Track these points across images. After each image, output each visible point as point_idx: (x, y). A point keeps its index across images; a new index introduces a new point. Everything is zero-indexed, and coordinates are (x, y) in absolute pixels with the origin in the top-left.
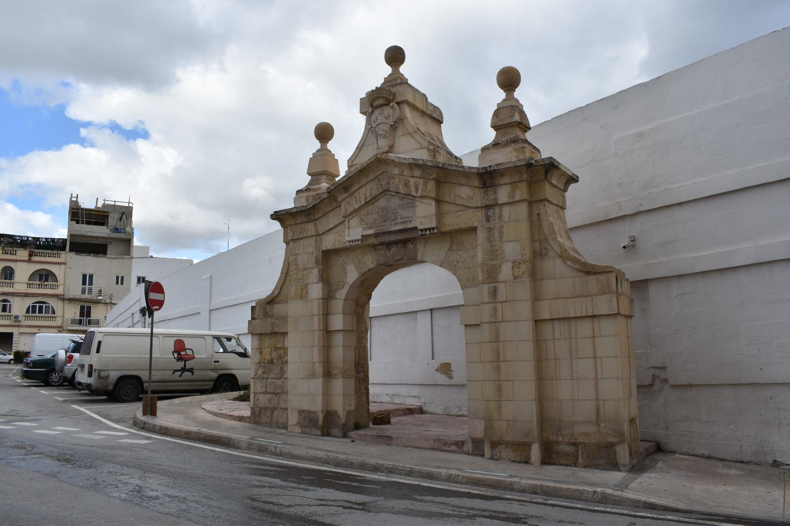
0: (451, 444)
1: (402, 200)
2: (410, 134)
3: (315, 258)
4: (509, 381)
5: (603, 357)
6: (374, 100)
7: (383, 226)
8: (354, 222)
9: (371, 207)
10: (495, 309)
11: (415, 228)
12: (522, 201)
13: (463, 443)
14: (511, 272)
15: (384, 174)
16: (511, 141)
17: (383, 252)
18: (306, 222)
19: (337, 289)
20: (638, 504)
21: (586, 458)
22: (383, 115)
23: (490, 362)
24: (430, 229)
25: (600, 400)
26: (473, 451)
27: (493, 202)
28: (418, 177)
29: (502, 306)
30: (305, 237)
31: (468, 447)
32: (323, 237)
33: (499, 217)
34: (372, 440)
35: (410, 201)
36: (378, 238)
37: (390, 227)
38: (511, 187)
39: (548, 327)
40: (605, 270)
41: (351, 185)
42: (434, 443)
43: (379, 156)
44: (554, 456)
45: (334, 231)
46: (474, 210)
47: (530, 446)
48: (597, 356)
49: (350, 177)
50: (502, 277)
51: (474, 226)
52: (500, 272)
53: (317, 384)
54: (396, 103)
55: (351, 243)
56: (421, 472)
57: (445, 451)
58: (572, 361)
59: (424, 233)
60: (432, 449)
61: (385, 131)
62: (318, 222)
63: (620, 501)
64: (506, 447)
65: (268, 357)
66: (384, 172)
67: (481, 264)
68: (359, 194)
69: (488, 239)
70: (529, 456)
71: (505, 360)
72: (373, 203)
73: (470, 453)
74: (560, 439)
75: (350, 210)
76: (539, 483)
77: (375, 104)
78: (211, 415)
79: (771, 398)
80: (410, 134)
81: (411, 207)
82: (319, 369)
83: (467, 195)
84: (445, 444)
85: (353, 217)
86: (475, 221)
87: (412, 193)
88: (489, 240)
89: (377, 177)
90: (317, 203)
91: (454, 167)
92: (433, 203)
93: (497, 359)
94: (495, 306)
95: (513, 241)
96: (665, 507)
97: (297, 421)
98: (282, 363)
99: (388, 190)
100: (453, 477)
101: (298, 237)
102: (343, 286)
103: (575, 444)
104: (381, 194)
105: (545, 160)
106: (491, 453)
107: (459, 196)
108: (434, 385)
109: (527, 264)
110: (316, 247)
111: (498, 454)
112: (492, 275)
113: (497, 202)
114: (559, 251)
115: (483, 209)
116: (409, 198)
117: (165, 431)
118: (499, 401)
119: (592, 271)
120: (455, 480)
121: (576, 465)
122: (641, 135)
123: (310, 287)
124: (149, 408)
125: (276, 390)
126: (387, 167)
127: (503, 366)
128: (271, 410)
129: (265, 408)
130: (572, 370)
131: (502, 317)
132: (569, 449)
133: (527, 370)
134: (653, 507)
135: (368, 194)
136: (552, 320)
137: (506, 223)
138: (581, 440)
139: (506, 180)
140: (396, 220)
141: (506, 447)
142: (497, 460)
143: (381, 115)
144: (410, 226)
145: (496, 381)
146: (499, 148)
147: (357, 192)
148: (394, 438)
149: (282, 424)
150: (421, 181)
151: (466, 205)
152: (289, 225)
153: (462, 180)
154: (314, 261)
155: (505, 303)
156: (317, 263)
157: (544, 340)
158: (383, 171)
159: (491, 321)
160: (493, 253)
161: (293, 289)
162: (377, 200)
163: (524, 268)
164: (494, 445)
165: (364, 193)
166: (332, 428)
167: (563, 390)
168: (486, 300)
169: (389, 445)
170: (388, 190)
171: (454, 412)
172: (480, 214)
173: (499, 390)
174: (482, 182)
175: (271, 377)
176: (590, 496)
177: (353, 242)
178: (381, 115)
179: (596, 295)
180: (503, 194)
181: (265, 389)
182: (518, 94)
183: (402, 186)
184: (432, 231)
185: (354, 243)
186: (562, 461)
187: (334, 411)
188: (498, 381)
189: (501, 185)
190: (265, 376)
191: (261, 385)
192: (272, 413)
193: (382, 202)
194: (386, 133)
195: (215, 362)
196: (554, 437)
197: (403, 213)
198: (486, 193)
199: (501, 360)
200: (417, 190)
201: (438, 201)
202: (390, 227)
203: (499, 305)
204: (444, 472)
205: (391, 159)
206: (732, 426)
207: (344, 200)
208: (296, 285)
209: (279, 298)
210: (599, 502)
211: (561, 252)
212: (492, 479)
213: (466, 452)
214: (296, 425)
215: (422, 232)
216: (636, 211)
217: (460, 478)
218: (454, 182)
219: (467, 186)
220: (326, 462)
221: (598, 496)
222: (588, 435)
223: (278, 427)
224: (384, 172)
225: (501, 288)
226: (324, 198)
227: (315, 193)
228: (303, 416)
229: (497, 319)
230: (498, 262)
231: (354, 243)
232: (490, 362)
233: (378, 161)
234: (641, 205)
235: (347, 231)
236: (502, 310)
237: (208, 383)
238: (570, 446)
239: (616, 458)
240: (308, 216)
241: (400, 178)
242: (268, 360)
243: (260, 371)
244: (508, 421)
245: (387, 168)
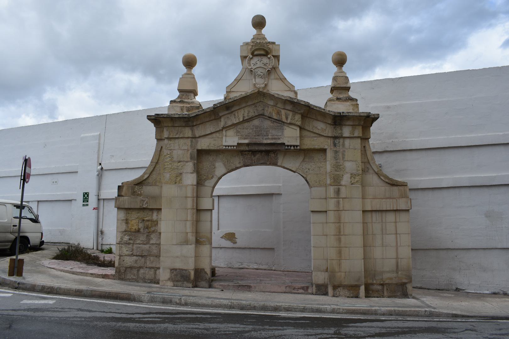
0: (298, 288)
1: (273, 123)
2: (281, 79)
3: (191, 154)
4: (347, 247)
6: (256, 50)
7: (256, 139)
8: (231, 132)
9: (246, 125)
10: (338, 202)
11: (284, 144)
12: (358, 137)
14: (349, 180)
19: (205, 180)
21: (390, 292)
22: (262, 62)
23: (334, 235)
24: (294, 146)
25: (399, 258)
26: (316, 292)
27: (339, 135)
29: (343, 201)
30: (181, 138)
32: (199, 139)
33: (342, 145)
38: (352, 128)
41: (232, 106)
43: (260, 90)
44: (371, 292)
45: (210, 136)
47: (359, 287)
49: (235, 100)
50: (343, 183)
51: (325, 148)
52: (343, 179)
53: (190, 249)
54: (272, 55)
55: (227, 147)
56: (312, 308)
57: (294, 293)
59: (289, 148)
62: (195, 128)
67: (330, 173)
69: (335, 157)
70: (358, 293)
72: (248, 122)
74: (375, 282)
75: (230, 123)
77: (256, 53)
78: (71, 274)
79: (456, 256)
80: (281, 79)
81: (280, 129)
83: (321, 128)
84: (294, 289)
85: (230, 129)
86: (325, 145)
88: (336, 158)
93: (339, 234)
94: (338, 200)
96: (463, 315)
99: (263, 115)
100: (336, 310)
101: (174, 137)
104: (256, 116)
106: (333, 293)
107: (316, 127)
108: (219, 247)
109: (360, 176)
110: (191, 146)
111: (338, 293)
112: (337, 181)
113: (342, 136)
118: (340, 260)
119: (396, 184)
120: (337, 312)
121: (383, 297)
122: (388, 107)
124: (16, 270)
125: (143, 253)
127: (343, 238)
129: (131, 268)
130: (383, 241)
131: (343, 207)
133: (358, 241)
134: (457, 316)
135: (246, 115)
136: (372, 211)
138: (387, 282)
142: (337, 297)
148: (253, 287)
149: (149, 279)
150: (291, 114)
157: (366, 223)
159: (335, 209)
160: (338, 167)
161: (167, 176)
164: (335, 287)
166: (199, 282)
167: (377, 253)
168: (332, 196)
169: (249, 291)
173: (340, 253)
174: (333, 121)
176: (423, 313)
180: (346, 131)
184: (296, 148)
185: (230, 148)
186: (375, 295)
188: (340, 247)
189: (345, 125)
190: (131, 242)
192: (138, 271)
193: (256, 122)
194: (263, 75)
195: (14, 226)
196: (371, 281)
197: (274, 132)
200: (287, 118)
203: (341, 200)
204: (328, 307)
208: (170, 173)
209: (147, 181)
214: (167, 280)
215: (288, 147)
217: (341, 310)
218: (313, 118)
223: (145, 282)
225: (343, 189)
227: (189, 106)
228: (175, 273)
231: (230, 148)
232: (334, 235)
235: (224, 138)
236: (343, 203)
237: (7, 244)
239: (407, 291)
242: (136, 229)
243: (126, 238)
245: (263, 99)
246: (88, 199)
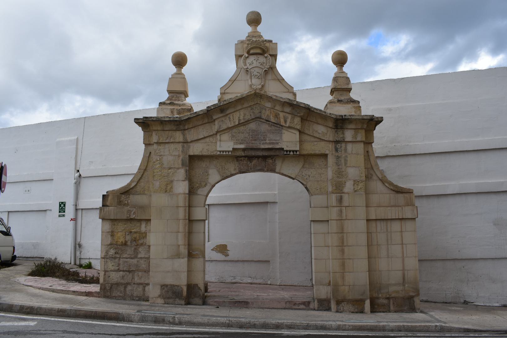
3: (182, 160)
5: (408, 244)
7: (252, 143)
8: (226, 137)
9: (242, 128)
12: (361, 141)
13: (309, 303)
14: (352, 188)
15: (258, 105)
17: (245, 162)
18: (175, 130)
19: (198, 188)
20: (461, 330)
21: (396, 307)
22: (258, 61)
24: (293, 151)
26: (318, 308)
28: (288, 113)
30: (172, 142)
31: (316, 304)
32: (191, 144)
34: (230, 306)
35: (278, 128)
36: (246, 152)
37: (259, 145)
38: (355, 132)
39: (373, 224)
40: (408, 191)
41: (228, 109)
42: (286, 304)
43: (257, 91)
44: (376, 306)
45: (203, 141)
46: (327, 142)
47: (364, 301)
48: (404, 243)
50: (346, 190)
55: (222, 153)
58: (388, 246)
60: (285, 309)
61: (260, 73)
62: (186, 132)
63: (451, 329)
64: (347, 303)
65: (122, 240)
68: (233, 116)
69: (337, 163)
70: (363, 308)
71: (348, 245)
72: (244, 125)
74: (380, 296)
75: (224, 127)
76: (401, 324)
77: (252, 52)
79: (464, 267)
80: (278, 80)
81: (279, 133)
82: (184, 251)
84: (295, 304)
85: (224, 133)
86: (327, 150)
87: (281, 123)
88: (338, 164)
89: (251, 106)
90: (192, 117)
93: (342, 246)
95: (354, 167)
96: (475, 330)
97: (160, 294)
98: (137, 245)
99: (260, 118)
102: (206, 185)
105: (379, 118)
106: (337, 308)
108: (210, 261)
111: (342, 308)
112: (339, 188)
114: (380, 177)
115: (333, 143)
116: (278, 126)
117: (28, 310)
119: (401, 191)
120: (343, 328)
121: (389, 312)
122: (390, 110)
123: (175, 183)
125: (130, 268)
126: (261, 100)
127: (346, 249)
129: (118, 284)
132: (385, 301)
133: (363, 252)
135: (242, 118)
136: (376, 220)
137: (349, 154)
138: (393, 295)
139: (352, 126)
141: (347, 303)
142: (341, 312)
143: (257, 61)
144: (278, 147)
145: (341, 259)
146: (342, 104)
147: (231, 115)
149: (137, 297)
150: (290, 117)
151: (322, 138)
152: (155, 130)
153: (320, 121)
154: (180, 162)
155: (348, 208)
156: (183, 164)
157: (370, 233)
158: (256, 102)
159: (337, 219)
160: (340, 173)
162: (248, 124)
163: (361, 185)
164: (338, 303)
165: (237, 116)
166: (193, 298)
167: (382, 264)
168: (334, 204)
169: (247, 308)
170: (260, 118)
171: (229, 280)
173: (343, 265)
174: (335, 125)
175: (124, 257)
176: (434, 328)
179: (405, 206)
180: (349, 135)
181: (118, 268)
182: (346, 68)
184: (295, 153)
187: (194, 285)
188: (343, 259)
189: (347, 129)
191: (113, 264)
192: (125, 287)
193: (253, 126)
196: (376, 295)
198: (337, 132)
199: (344, 245)
200: (286, 122)
202: (259, 145)
203: (344, 208)
205: (269, 95)
206: (441, 283)
207: (218, 118)
209: (134, 189)
210: (439, 332)
211: (382, 178)
212: (370, 325)
213: (312, 308)
214: (158, 297)
216: (386, 155)
217: (347, 327)
219: (323, 125)
220: (229, 326)
221: (438, 328)
222: (397, 292)
223: (133, 300)
224: (257, 103)
225: (345, 197)
226: (200, 114)
227: (180, 108)
229: (342, 217)
230: (344, 180)
233: (255, 95)
234: (389, 152)
235: (218, 143)
238: (386, 300)
239: (414, 305)
240: (177, 125)
241: (271, 110)
243: (112, 252)
244: (350, 286)
245: (260, 101)
246: (65, 209)
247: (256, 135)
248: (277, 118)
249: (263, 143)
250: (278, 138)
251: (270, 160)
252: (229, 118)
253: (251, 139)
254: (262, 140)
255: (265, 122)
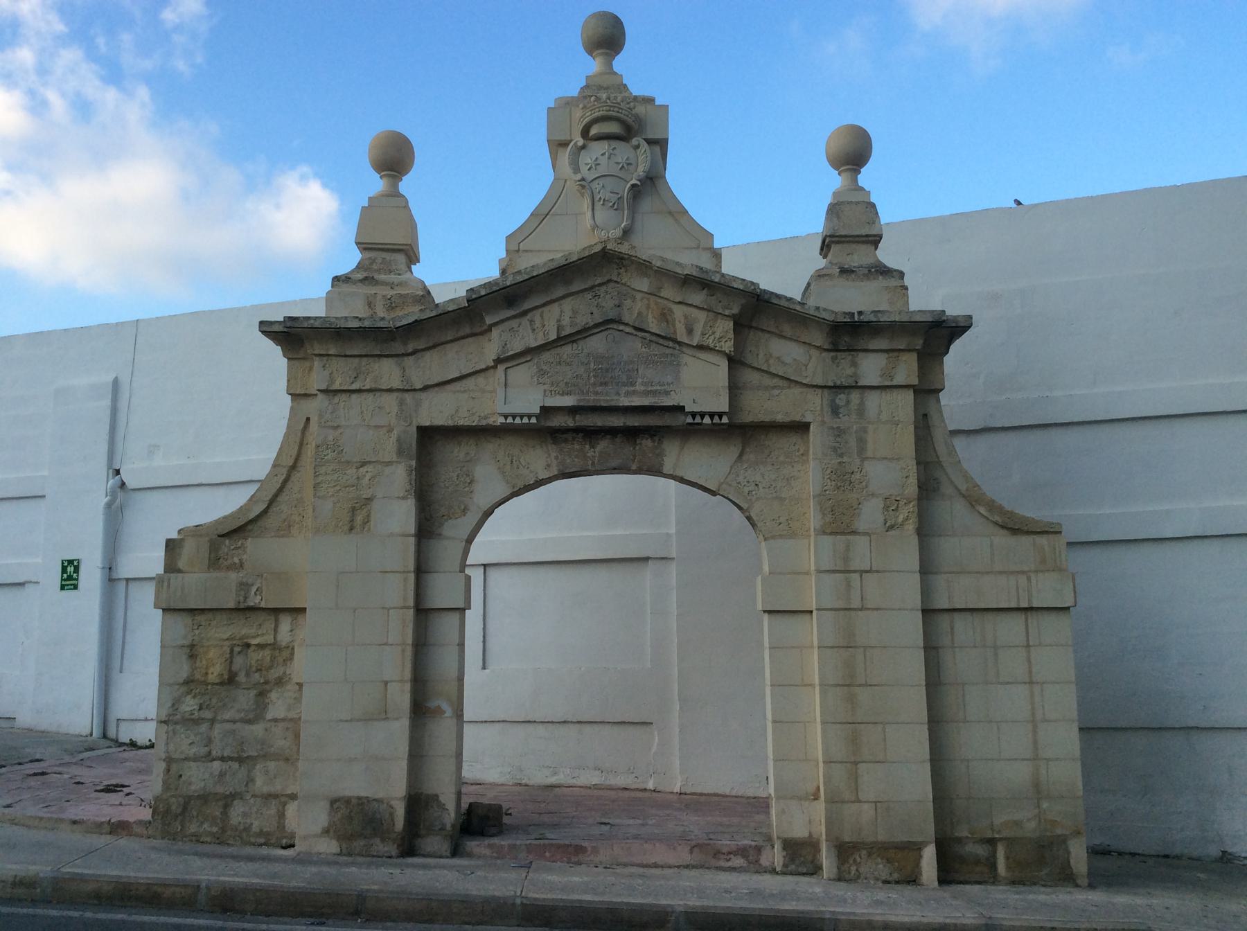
0: (730, 853)
9: (567, 350)
11: (680, 409)
15: (612, 284)
16: (876, 271)
24: (712, 415)
26: (785, 866)
35: (668, 351)
47: (920, 849)
51: (804, 420)
66: (609, 281)
72: (573, 342)
73: (778, 869)
75: (517, 346)
77: (594, 131)
91: (784, 300)
92: (724, 364)
103: (992, 842)
104: (597, 325)
113: (857, 382)
123: (376, 505)
125: (243, 751)
126: (622, 270)
128: (221, 803)
129: (204, 798)
135: (566, 321)
140: (633, 384)
144: (668, 402)
149: (261, 833)
150: (701, 316)
162: (587, 337)
172: (818, 401)
177: (522, 417)
178: (609, 158)
183: (654, 317)
184: (716, 420)
190: (207, 714)
192: (226, 807)
193: (597, 344)
200: (690, 331)
201: (735, 362)
203: (856, 576)
218: (769, 329)
224: (609, 281)
227: (392, 292)
238: (984, 846)
244: (876, 802)
245: (619, 274)
247: (607, 370)
248: (667, 322)
249: (628, 394)
250: (669, 379)
251: (647, 439)
252: (531, 321)
253: (592, 380)
254: (624, 385)
255: (632, 334)
